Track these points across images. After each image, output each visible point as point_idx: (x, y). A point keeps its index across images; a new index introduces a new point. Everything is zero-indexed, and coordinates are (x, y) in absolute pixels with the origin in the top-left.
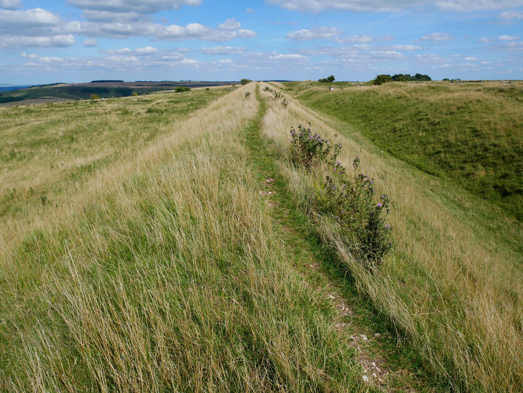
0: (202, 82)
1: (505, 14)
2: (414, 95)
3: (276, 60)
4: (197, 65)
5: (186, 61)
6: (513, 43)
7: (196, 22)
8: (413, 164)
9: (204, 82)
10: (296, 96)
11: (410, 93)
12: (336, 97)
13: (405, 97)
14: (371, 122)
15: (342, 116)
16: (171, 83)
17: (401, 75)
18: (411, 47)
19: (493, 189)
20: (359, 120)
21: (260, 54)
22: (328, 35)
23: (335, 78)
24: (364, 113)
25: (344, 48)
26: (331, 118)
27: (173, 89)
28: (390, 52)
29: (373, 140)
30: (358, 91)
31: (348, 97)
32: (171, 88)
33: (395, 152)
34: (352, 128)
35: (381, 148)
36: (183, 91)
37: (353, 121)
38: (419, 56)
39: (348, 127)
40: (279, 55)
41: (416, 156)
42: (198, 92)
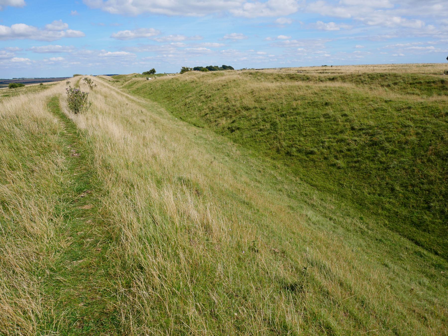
0: (36, 79)
1: (279, 20)
2: (202, 80)
3: (105, 57)
4: (28, 63)
5: (16, 59)
6: (288, 41)
7: (22, 22)
8: (192, 123)
9: (38, 79)
10: (122, 86)
11: (199, 78)
12: (151, 84)
13: (196, 81)
14: (173, 100)
15: (154, 98)
16: (3, 81)
17: (201, 67)
18: (216, 44)
19: (227, 130)
20: (165, 100)
21: (89, 52)
22: (149, 35)
23: (156, 71)
24: (169, 95)
25: (163, 46)
26: (146, 100)
27: (6, 87)
28: (201, 49)
29: (172, 113)
30: (166, 79)
31: (158, 84)
32: (4, 85)
33: (184, 118)
34: (159, 106)
35: (176, 116)
36: (16, 87)
37: (161, 101)
38: (224, 51)
39: (157, 106)
40: (107, 52)
41: (195, 119)
42: (32, 87)
